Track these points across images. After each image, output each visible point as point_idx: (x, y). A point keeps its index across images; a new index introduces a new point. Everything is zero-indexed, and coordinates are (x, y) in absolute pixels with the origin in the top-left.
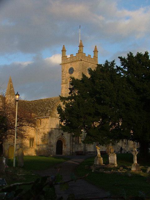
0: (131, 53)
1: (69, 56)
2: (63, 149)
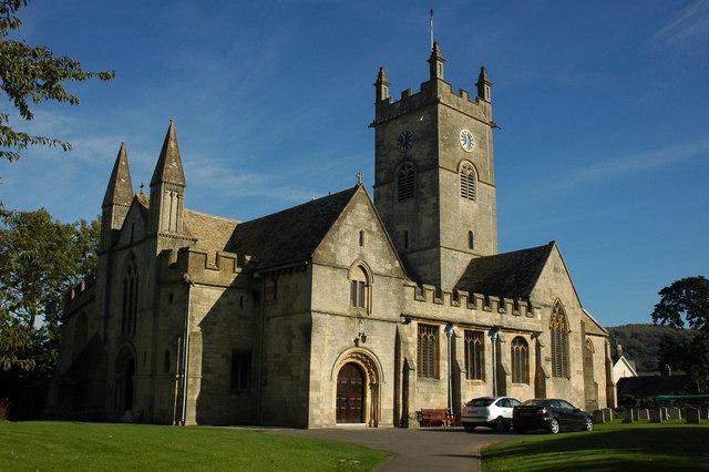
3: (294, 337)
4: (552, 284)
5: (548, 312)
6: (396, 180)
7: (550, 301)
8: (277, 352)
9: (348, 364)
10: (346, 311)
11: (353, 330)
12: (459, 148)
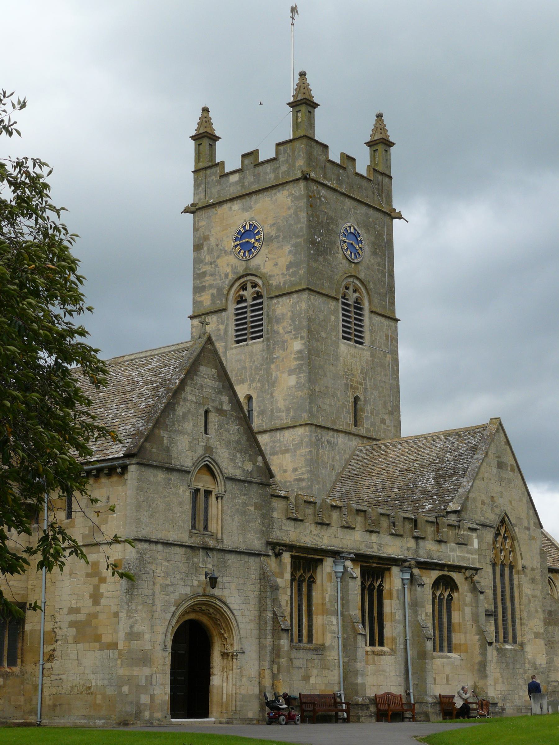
0: (296, 6)
1: (232, 163)
2: (216, 680)
3: (103, 580)
4: (495, 489)
5: (489, 535)
6: (232, 307)
7: (492, 518)
8: (74, 604)
9: (186, 622)
10: (185, 538)
11: (196, 569)
12: (340, 256)
